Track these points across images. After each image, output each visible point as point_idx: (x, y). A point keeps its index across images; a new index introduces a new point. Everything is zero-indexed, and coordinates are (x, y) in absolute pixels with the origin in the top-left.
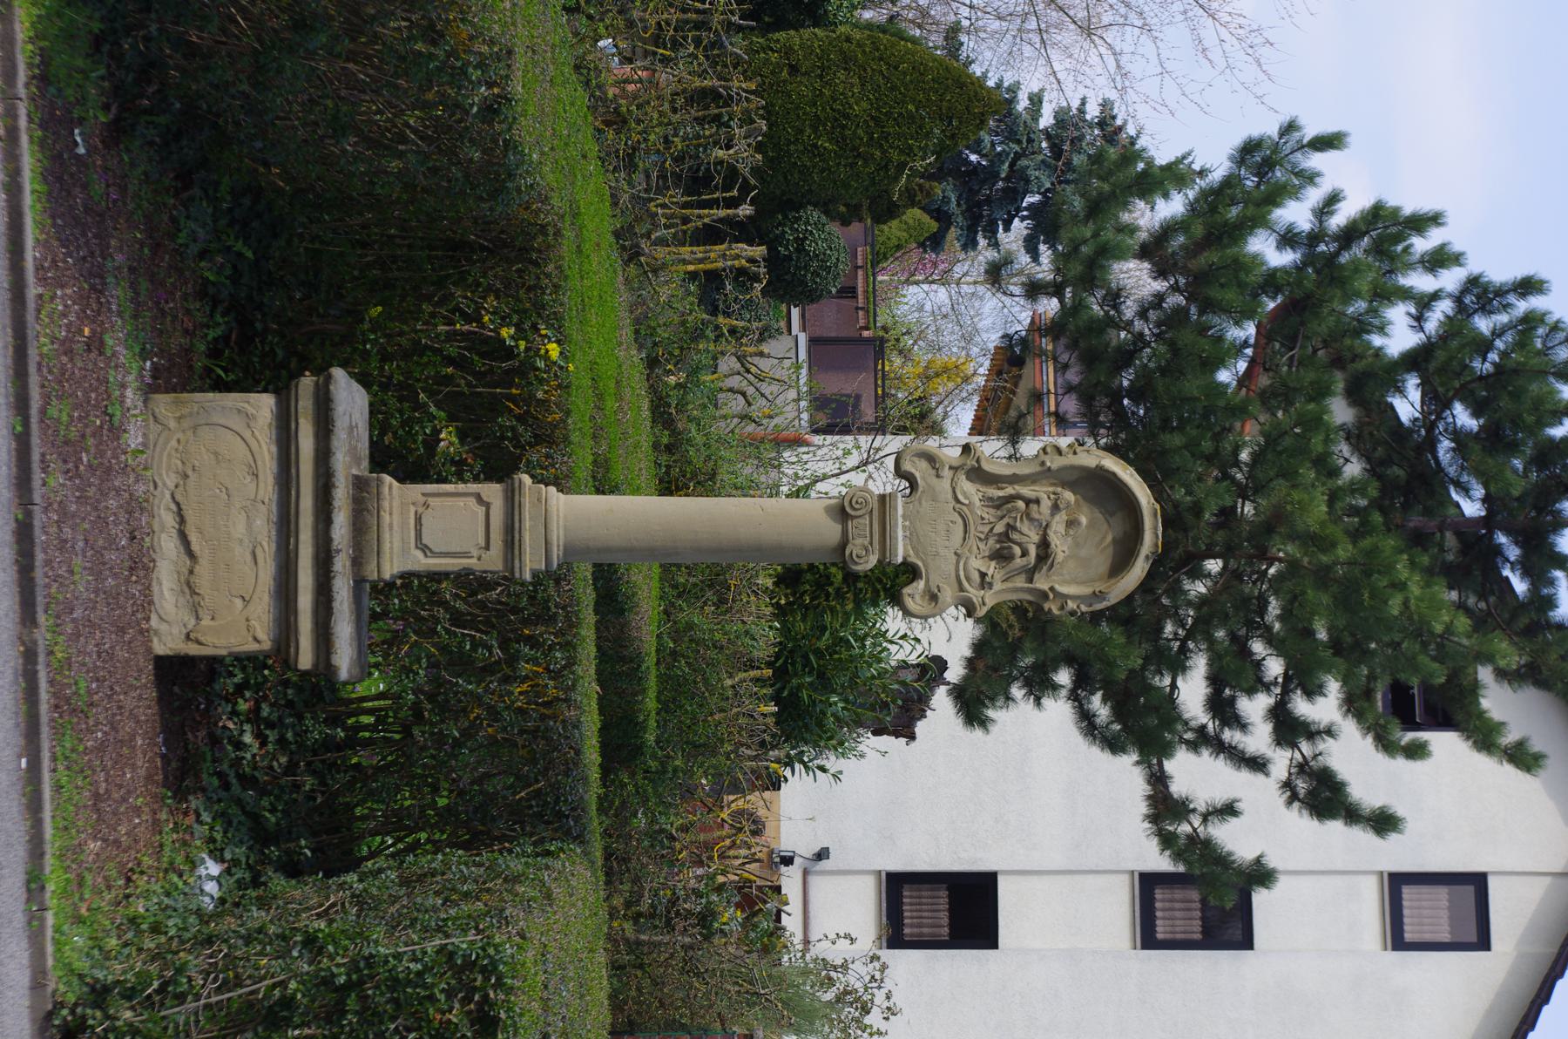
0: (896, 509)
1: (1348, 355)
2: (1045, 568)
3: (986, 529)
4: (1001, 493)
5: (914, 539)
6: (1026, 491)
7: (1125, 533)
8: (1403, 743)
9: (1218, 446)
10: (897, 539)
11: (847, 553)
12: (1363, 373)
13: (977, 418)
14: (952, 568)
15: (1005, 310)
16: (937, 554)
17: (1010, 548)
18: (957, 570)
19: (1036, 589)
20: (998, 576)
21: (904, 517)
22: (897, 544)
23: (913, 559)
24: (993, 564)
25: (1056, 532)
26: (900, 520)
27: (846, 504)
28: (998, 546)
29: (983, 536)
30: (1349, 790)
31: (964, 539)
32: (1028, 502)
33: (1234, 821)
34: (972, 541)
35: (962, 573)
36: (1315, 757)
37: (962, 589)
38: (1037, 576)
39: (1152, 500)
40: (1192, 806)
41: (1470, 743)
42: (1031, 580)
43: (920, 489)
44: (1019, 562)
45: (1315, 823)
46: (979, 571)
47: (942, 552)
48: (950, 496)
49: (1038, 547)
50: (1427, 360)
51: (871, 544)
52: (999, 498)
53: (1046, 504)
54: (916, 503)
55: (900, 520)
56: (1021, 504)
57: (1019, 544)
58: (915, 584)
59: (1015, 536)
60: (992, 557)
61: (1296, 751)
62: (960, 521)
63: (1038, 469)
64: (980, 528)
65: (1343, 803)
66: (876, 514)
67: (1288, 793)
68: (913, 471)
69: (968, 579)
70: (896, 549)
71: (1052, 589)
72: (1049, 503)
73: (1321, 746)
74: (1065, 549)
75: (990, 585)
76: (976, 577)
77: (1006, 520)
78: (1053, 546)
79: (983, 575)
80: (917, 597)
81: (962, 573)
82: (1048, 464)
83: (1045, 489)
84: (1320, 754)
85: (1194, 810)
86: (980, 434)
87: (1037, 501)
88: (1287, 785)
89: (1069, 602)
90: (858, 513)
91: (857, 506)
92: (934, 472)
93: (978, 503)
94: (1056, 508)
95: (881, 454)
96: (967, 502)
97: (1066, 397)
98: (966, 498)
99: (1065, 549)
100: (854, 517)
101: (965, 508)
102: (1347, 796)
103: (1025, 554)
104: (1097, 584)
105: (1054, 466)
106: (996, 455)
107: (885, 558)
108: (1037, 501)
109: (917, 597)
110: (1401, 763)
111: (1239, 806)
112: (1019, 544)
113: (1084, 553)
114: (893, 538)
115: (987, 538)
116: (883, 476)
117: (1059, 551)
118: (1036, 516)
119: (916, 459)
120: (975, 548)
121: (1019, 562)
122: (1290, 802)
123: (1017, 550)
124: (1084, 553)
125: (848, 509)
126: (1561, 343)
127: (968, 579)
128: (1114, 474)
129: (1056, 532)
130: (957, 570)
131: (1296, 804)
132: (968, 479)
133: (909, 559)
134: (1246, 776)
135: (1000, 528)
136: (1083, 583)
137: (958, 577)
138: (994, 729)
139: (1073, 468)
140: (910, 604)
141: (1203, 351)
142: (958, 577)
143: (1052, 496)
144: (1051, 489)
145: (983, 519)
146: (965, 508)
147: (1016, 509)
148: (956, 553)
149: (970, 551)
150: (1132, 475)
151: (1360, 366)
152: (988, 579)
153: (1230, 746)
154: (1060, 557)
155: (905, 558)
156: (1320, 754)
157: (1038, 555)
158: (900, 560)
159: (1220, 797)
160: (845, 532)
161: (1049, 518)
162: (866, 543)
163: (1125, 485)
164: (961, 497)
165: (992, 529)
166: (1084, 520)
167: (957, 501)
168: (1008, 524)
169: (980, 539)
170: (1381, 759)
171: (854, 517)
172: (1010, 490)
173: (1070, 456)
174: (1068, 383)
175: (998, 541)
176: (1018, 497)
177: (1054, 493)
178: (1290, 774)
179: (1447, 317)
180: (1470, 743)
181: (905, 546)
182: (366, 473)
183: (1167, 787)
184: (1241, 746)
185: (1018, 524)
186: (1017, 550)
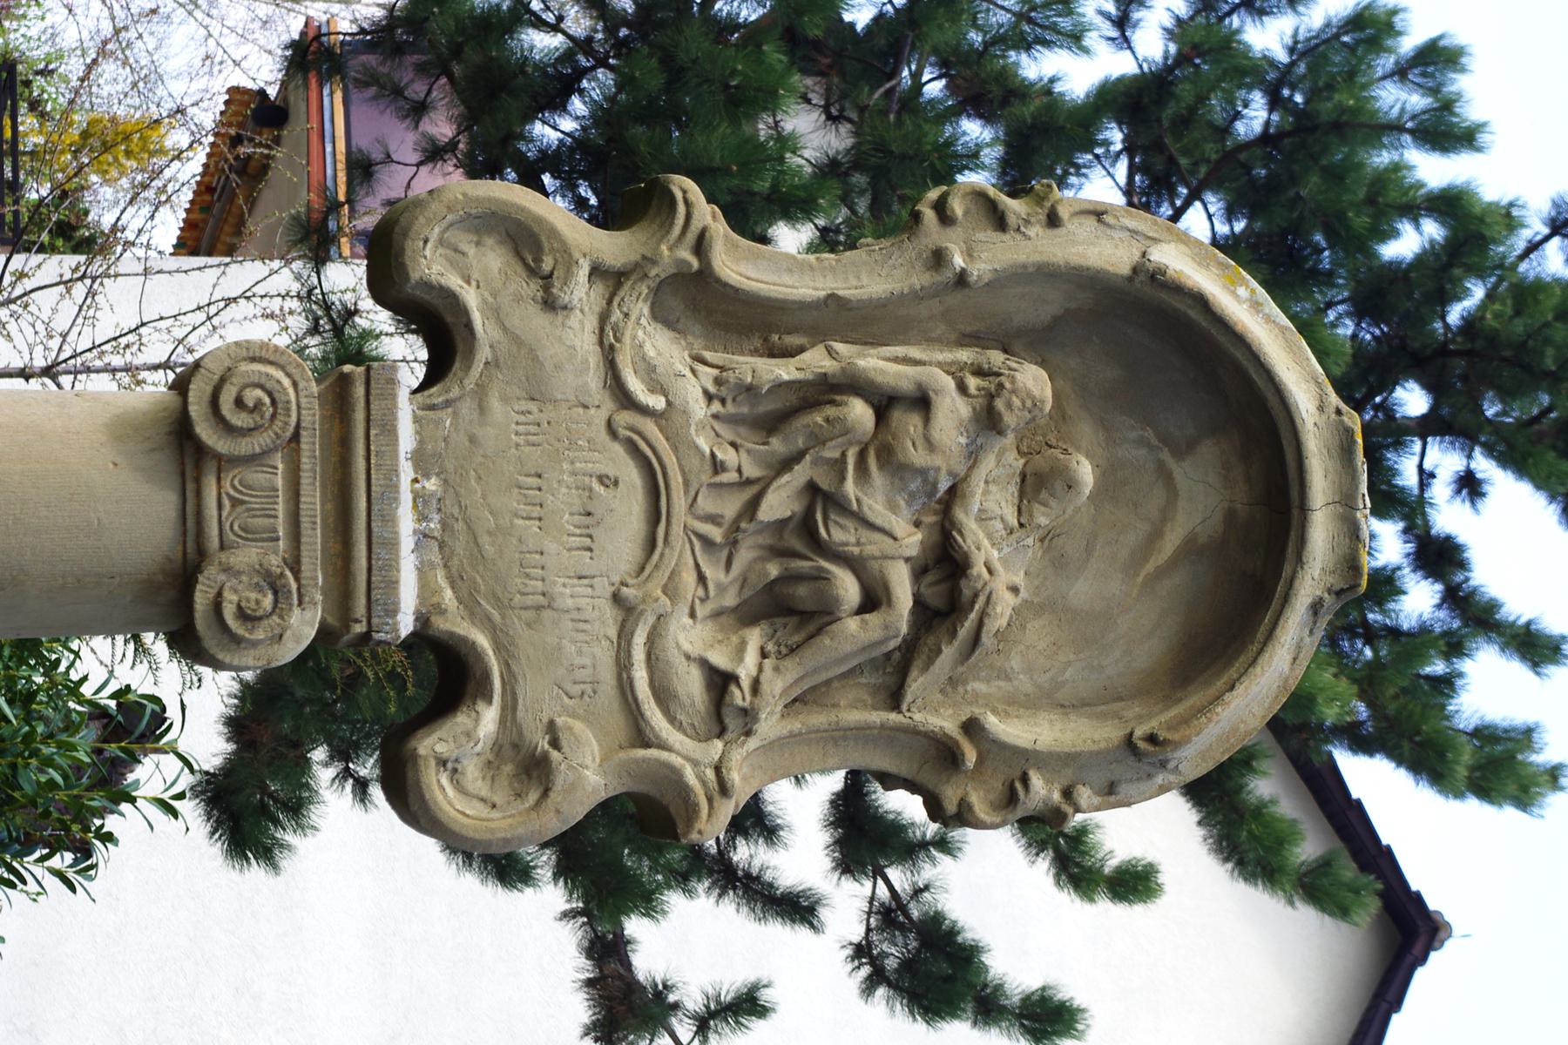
0: (391, 431)
1: (996, 90)
2: (949, 652)
3: (730, 507)
4: (785, 371)
5: (460, 546)
6: (876, 363)
7: (1230, 516)
8: (1107, 870)
9: (1419, 208)
10: (393, 545)
11: (201, 599)
12: (1033, 127)
13: (190, 226)
14: (604, 656)
15: (211, 42)
16: (548, 603)
17: (821, 577)
18: (623, 666)
19: (913, 732)
20: (776, 685)
21: (418, 458)
22: (393, 565)
23: (456, 623)
24: (755, 638)
25: (983, 518)
26: (406, 472)
27: (197, 410)
28: (773, 570)
29: (716, 534)
30: (986, 959)
31: (651, 544)
32: (885, 403)
33: (757, 1026)
34: (679, 554)
35: (640, 675)
36: (918, 892)
37: (641, 736)
38: (917, 684)
39: (1334, 399)
40: (672, 998)
41: (1229, 866)
42: (895, 699)
43: (483, 353)
44: (854, 631)
45: (920, 1026)
46: (705, 664)
47: (567, 593)
48: (594, 380)
49: (919, 572)
50: (1160, 102)
51: (295, 566)
52: (780, 386)
53: (952, 411)
54: (467, 408)
55: (406, 472)
56: (859, 412)
57: (854, 564)
58: (461, 719)
59: (840, 534)
60: (747, 615)
61: (880, 882)
62: (631, 475)
63: (920, 279)
64: (706, 504)
65: (972, 986)
66: (311, 446)
67: (866, 971)
68: (454, 282)
69: (663, 695)
70: (393, 584)
71: (972, 727)
72: (964, 409)
73: (927, 873)
74: (1019, 579)
75: (748, 716)
76: (692, 685)
77: (800, 474)
78: (979, 569)
79: (720, 681)
80: (472, 771)
81: (640, 675)
82: (959, 261)
83: (946, 356)
84: (927, 888)
85: (676, 1006)
86: (194, 252)
87: (922, 402)
88: (861, 951)
89: (1037, 781)
90: (245, 446)
91: (239, 420)
92: (533, 288)
93: (699, 410)
94: (988, 420)
95: (28, 284)
96: (658, 402)
97: (424, 170)
98: (657, 387)
99: (1019, 579)
100: (224, 463)
101: (650, 427)
102: (985, 969)
103: (873, 600)
104: (1133, 710)
105: (980, 270)
106: (259, 290)
107: (346, 616)
108: (922, 402)
109: (472, 771)
110: (1105, 910)
111: (765, 996)
112: (854, 564)
113: (1082, 591)
114: (381, 546)
115: (733, 543)
116: (29, 331)
117: (1000, 586)
118: (917, 456)
119: (466, 243)
120: (689, 577)
121: (854, 631)
122: (869, 987)
123: (848, 588)
124: (1082, 591)
125: (205, 431)
126: (1384, 78)
127: (663, 695)
128: (1201, 301)
129: (983, 518)
130: (623, 666)
131: (881, 992)
132: (660, 315)
133: (441, 625)
134: (780, 934)
135: (779, 503)
136: (1068, 707)
137: (625, 687)
138: (285, 862)
139: (1047, 274)
140: (441, 791)
141: (734, 72)
142: (625, 687)
143: (973, 382)
144: (965, 355)
145: (717, 466)
146: (650, 427)
147: (843, 429)
148: (617, 598)
149: (671, 590)
150: (1256, 306)
151: (1027, 111)
152: (739, 697)
153: (748, 875)
154: (1004, 606)
155: (423, 620)
156: (927, 888)
157: (918, 602)
158: (406, 624)
159: (730, 983)
160: (190, 520)
161: (961, 469)
162: (275, 562)
163: (1240, 340)
164: (635, 385)
165: (753, 506)
166: (1086, 472)
167: (626, 400)
168: (812, 489)
169: (707, 542)
170: (1067, 900)
171: (224, 463)
172: (816, 361)
173: (1034, 231)
174: (432, 140)
175: (779, 553)
176: (851, 384)
177: (979, 372)
178: (868, 930)
179: (1179, 21)
180: (1229, 866)
181: (422, 571)
182: (1010, 439)
183: (628, 965)
184: (768, 876)
185: (850, 488)
186: (848, 588)
